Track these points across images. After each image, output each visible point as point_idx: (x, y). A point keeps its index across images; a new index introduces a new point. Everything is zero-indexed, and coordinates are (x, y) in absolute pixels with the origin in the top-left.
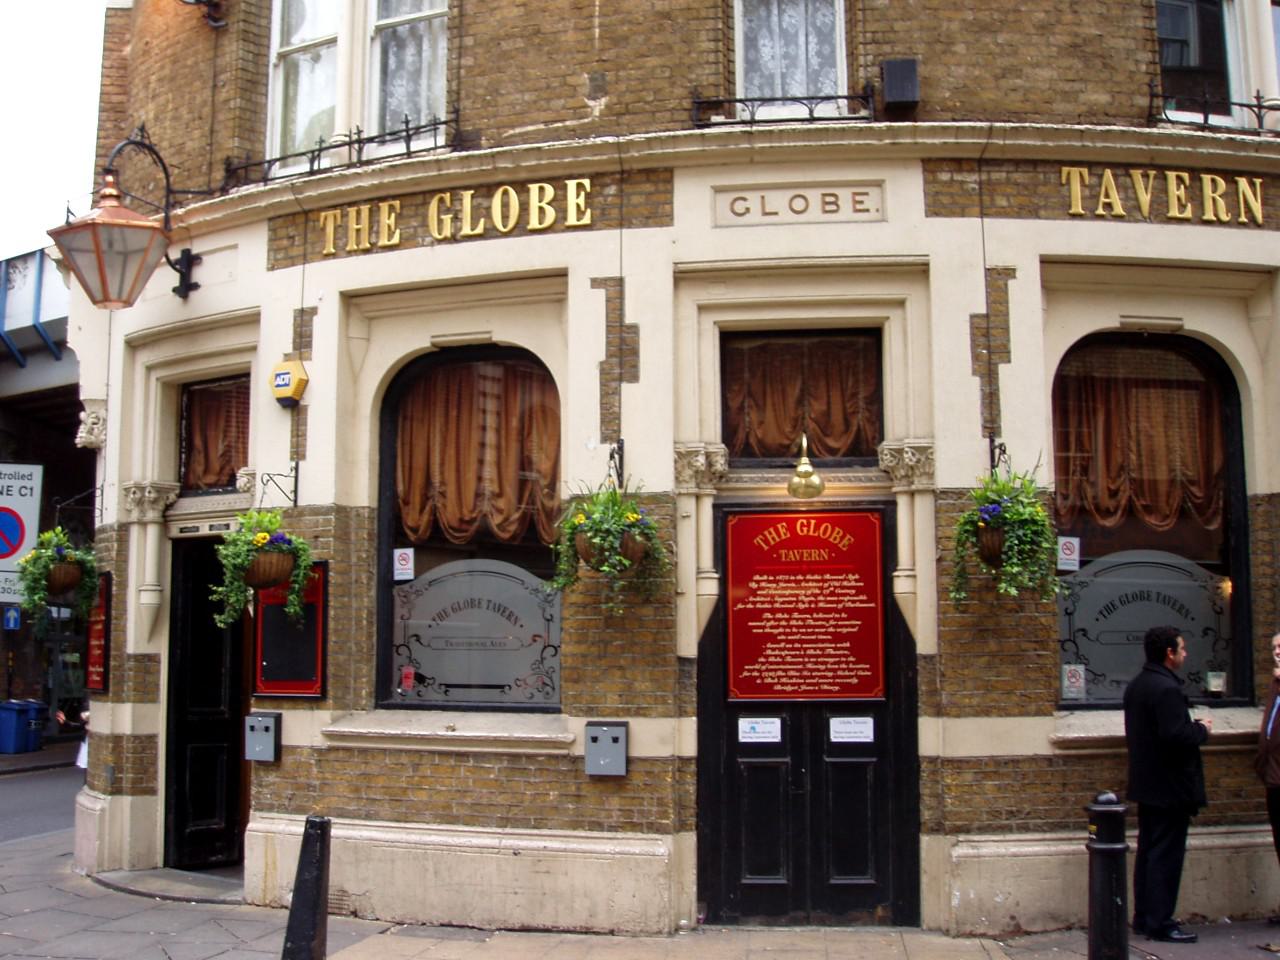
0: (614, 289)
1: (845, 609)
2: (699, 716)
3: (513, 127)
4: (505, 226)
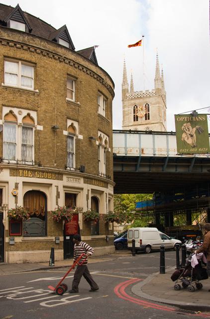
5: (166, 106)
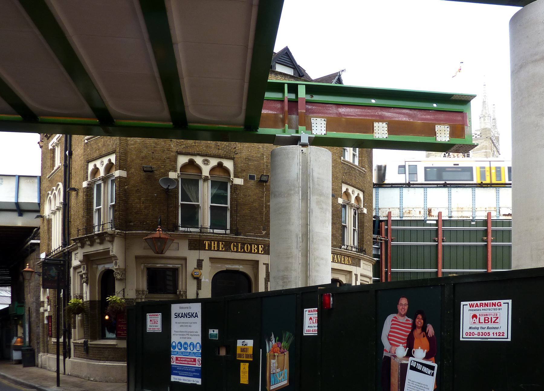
2: (26, 341)
4: (247, 251)
5: (498, 152)
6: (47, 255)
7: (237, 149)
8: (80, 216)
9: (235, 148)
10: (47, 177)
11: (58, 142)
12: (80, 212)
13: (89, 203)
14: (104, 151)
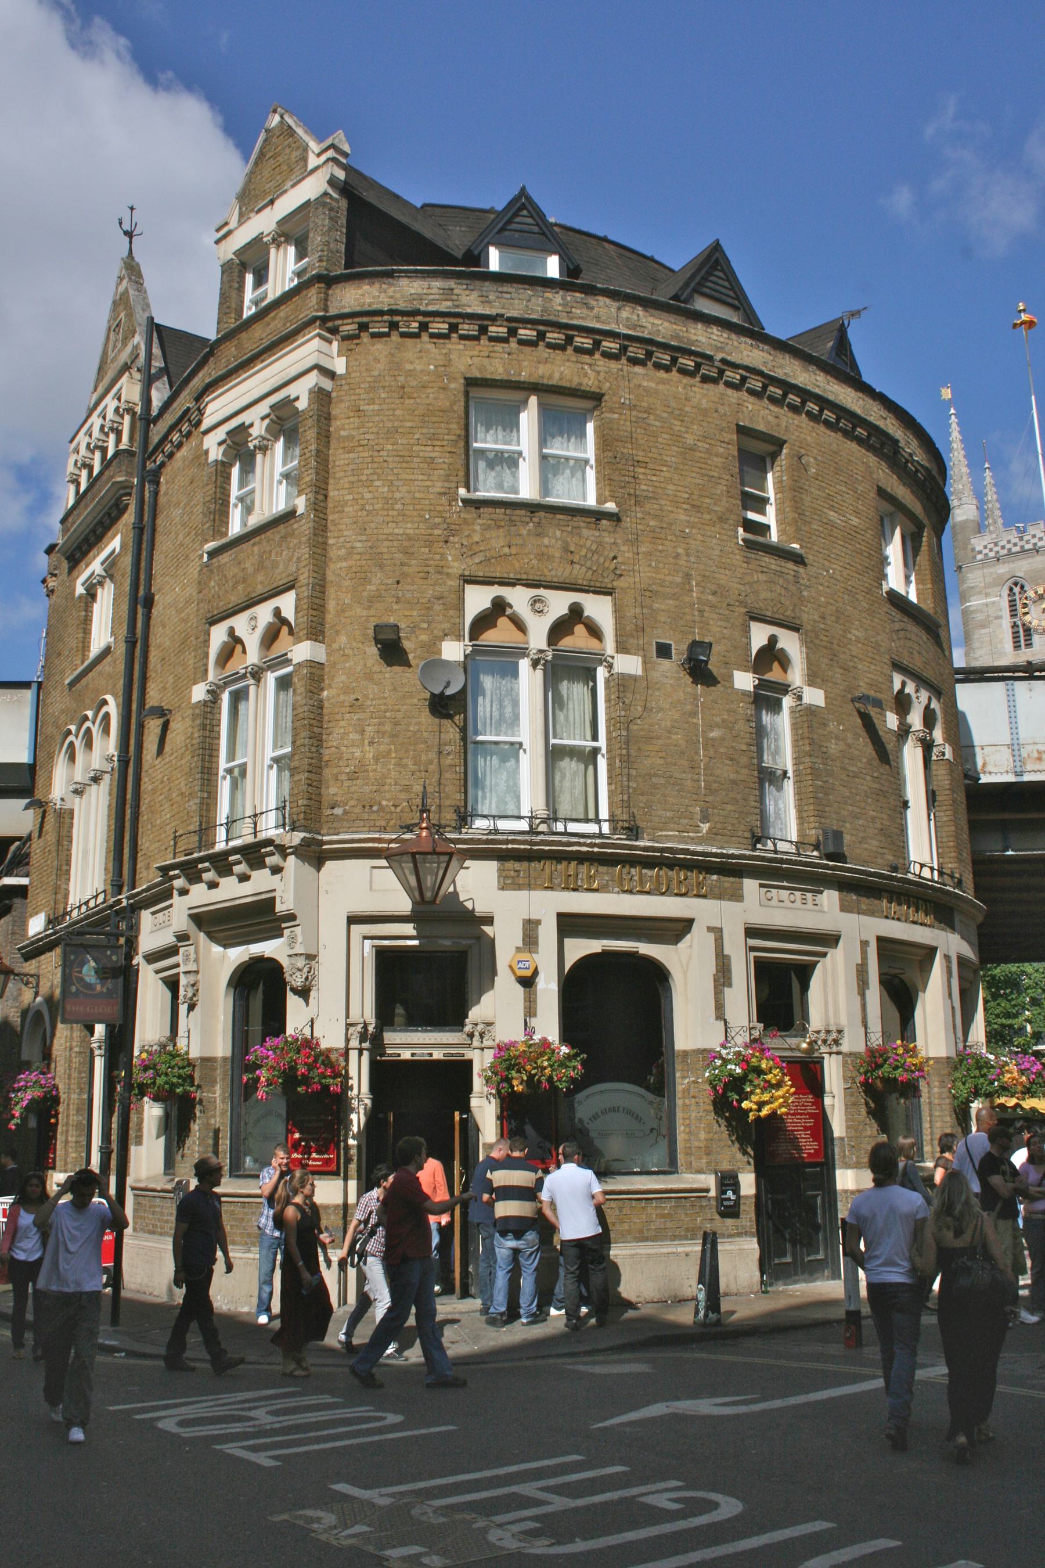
0: (717, 932)
1: (808, 1114)
3: (661, 830)
6: (50, 922)
7: (620, 559)
8: (174, 795)
9: (615, 558)
10: (67, 681)
11: (104, 574)
12: (176, 782)
13: (207, 752)
14: (259, 587)
